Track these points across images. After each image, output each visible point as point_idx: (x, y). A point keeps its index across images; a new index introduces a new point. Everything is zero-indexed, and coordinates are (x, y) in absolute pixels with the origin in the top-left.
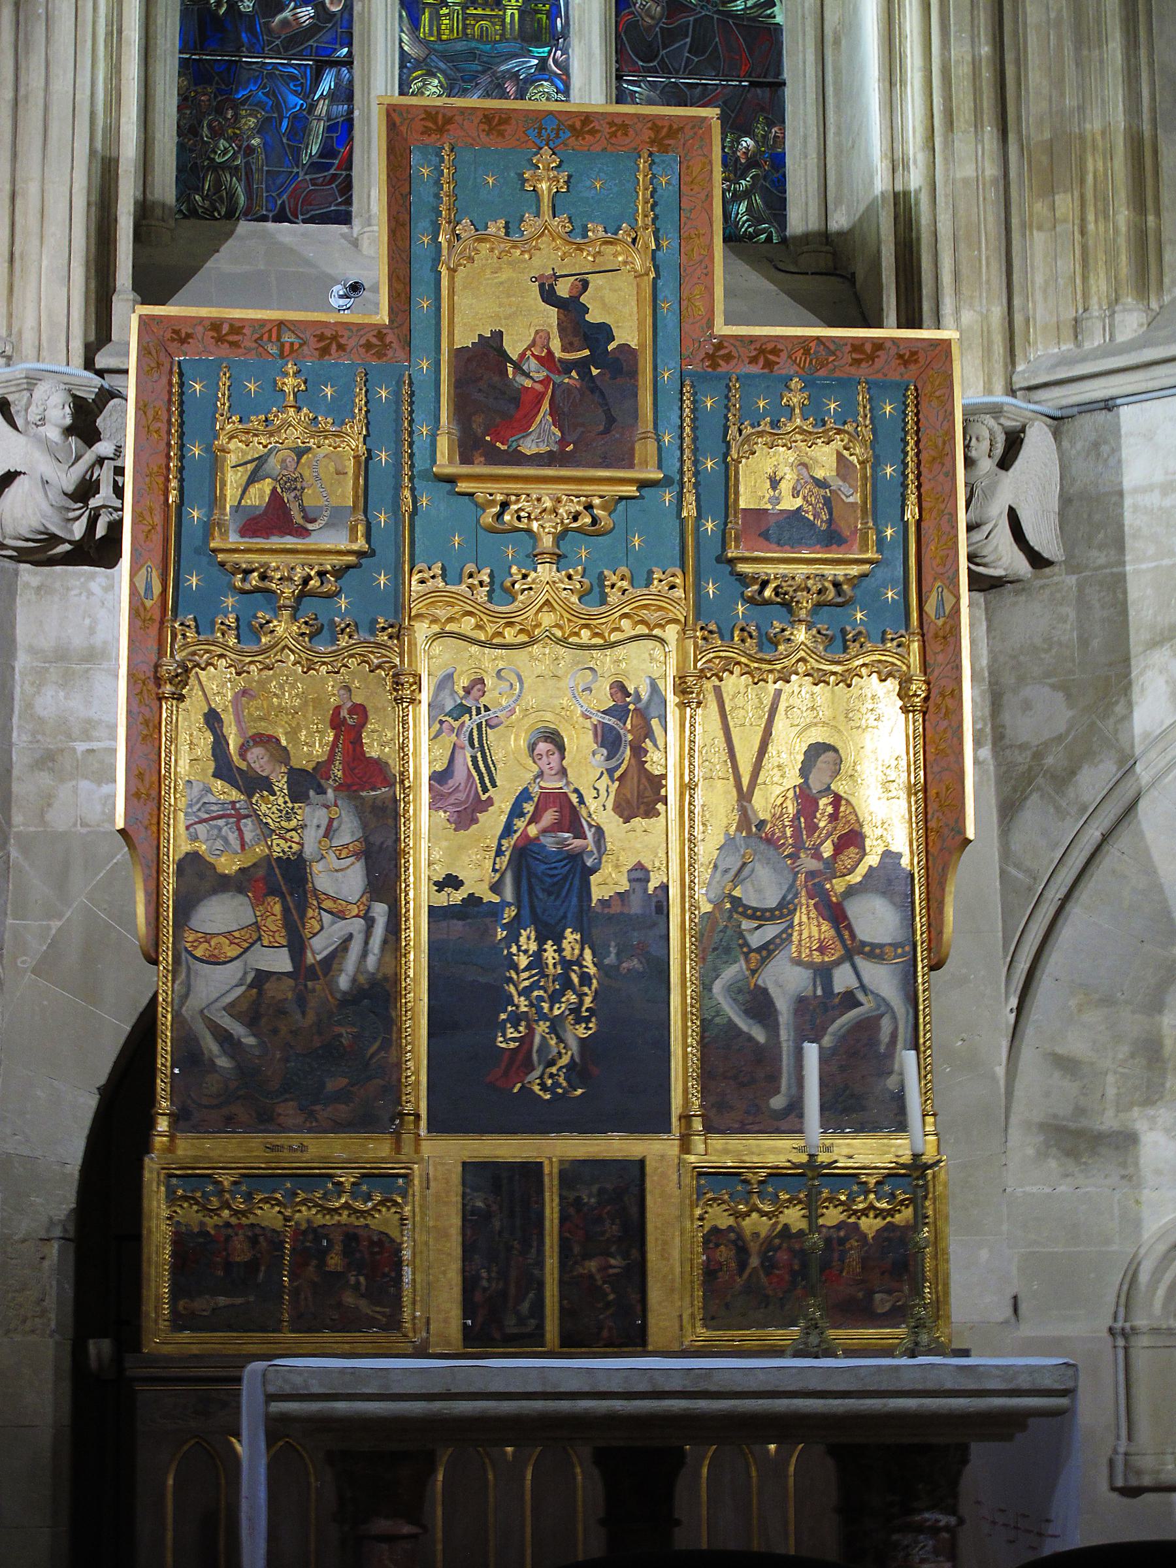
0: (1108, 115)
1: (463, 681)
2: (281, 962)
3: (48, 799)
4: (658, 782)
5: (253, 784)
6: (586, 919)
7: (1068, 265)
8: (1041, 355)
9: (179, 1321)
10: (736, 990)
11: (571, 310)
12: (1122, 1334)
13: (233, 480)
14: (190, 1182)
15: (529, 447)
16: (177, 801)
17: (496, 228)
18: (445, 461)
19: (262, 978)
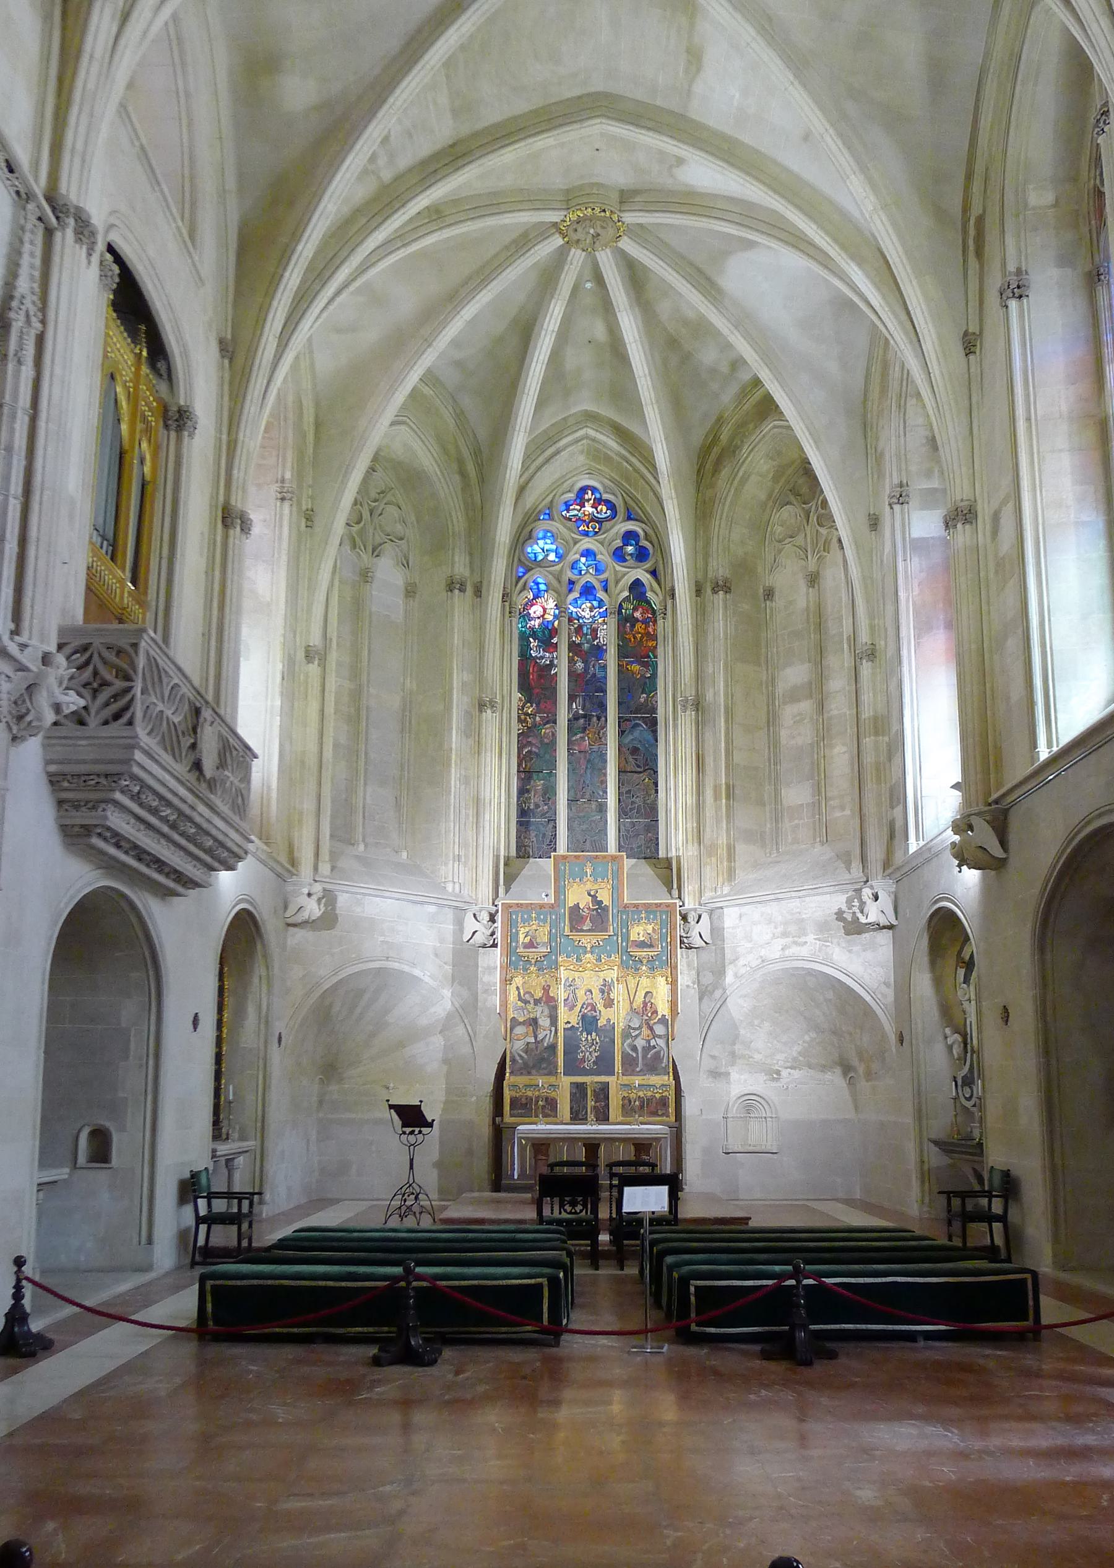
0: (723, 840)
3: (486, 1000)
5: (526, 1002)
8: (708, 895)
9: (512, 1116)
10: (629, 1045)
11: (594, 897)
13: (521, 936)
14: (514, 1086)
15: (585, 928)
17: (578, 880)
18: (567, 931)
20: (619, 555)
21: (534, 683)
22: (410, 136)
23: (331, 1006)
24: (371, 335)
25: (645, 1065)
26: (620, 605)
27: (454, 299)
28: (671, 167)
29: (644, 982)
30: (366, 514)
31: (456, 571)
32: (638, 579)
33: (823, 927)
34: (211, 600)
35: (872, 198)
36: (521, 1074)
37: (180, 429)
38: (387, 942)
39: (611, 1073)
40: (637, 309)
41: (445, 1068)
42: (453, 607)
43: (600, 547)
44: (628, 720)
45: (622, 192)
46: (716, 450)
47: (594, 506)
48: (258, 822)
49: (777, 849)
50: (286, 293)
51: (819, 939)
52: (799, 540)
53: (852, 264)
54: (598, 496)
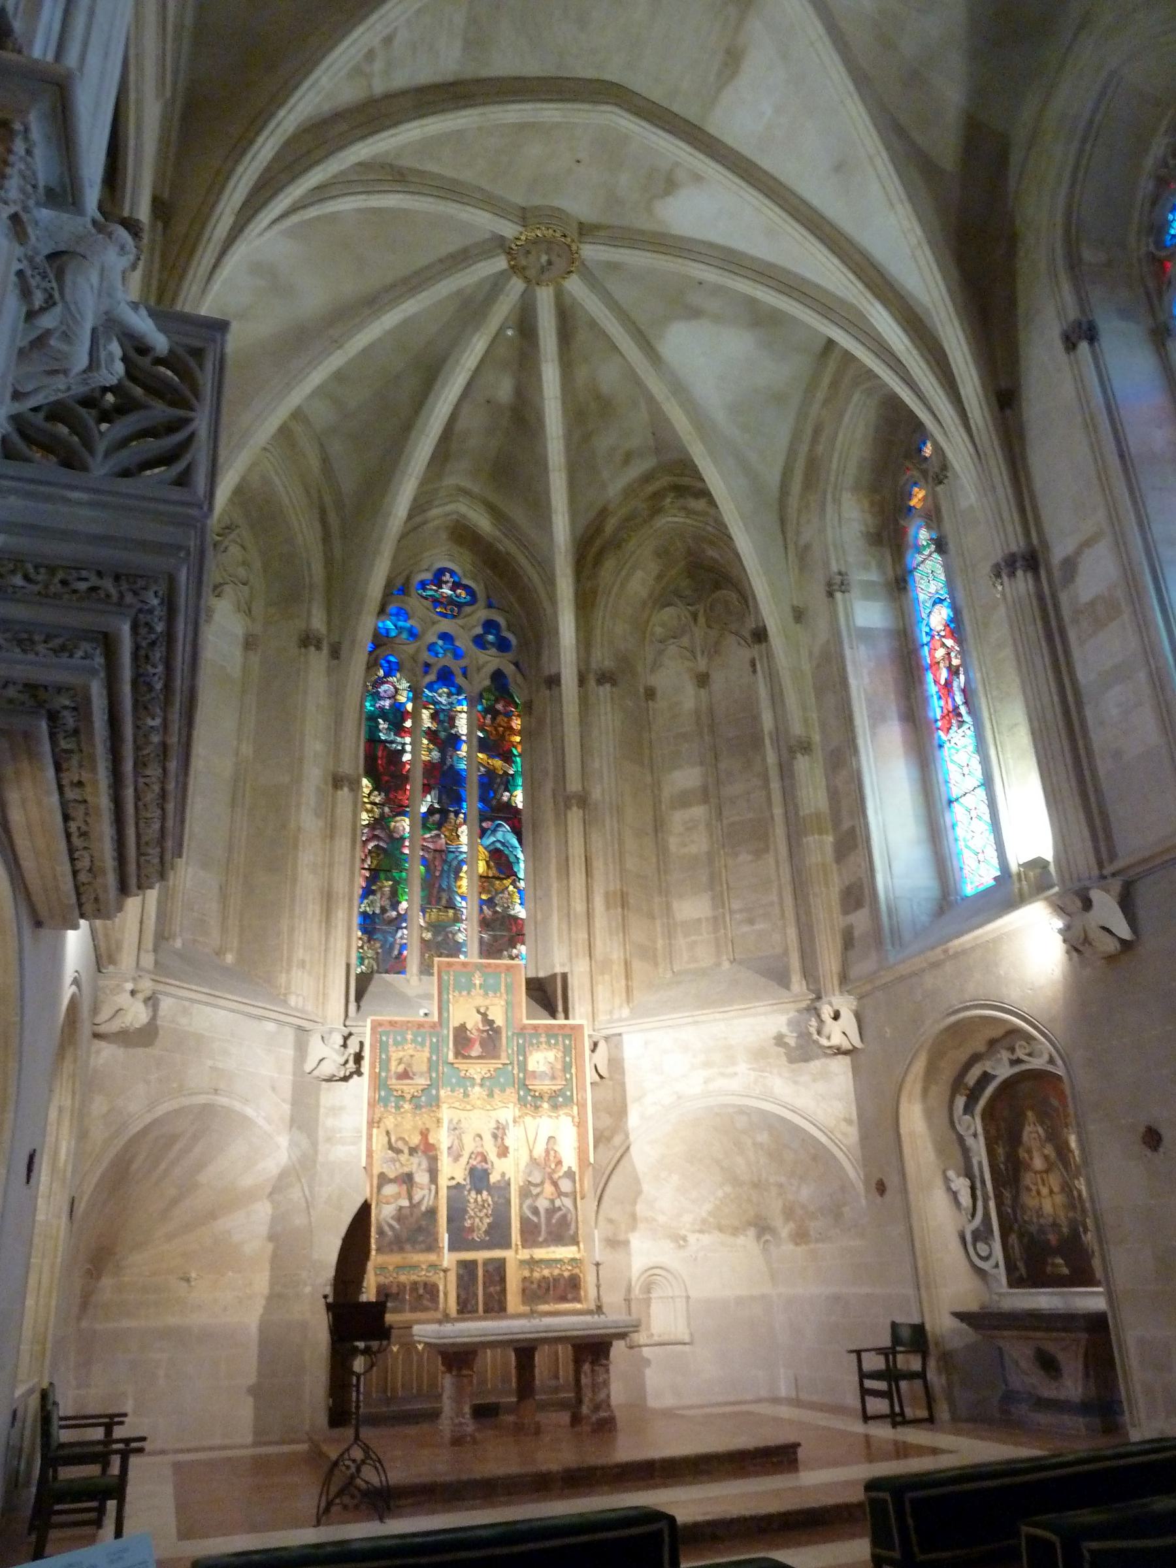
0: (617, 955)
1: (455, 1121)
2: (406, 1203)
4: (507, 1148)
5: (398, 1151)
6: (489, 1188)
11: (484, 1015)
12: (628, 1301)
13: (393, 1064)
15: (473, 1054)
17: (464, 993)
19: (401, 1208)
20: (479, 641)
25: (550, 1233)
27: (373, 303)
33: (758, 1055)
36: (392, 1251)
39: (506, 1244)
41: (270, 1247)
43: (465, 629)
46: (598, 543)
47: (453, 589)
51: (754, 1069)
52: (685, 641)
54: (457, 579)
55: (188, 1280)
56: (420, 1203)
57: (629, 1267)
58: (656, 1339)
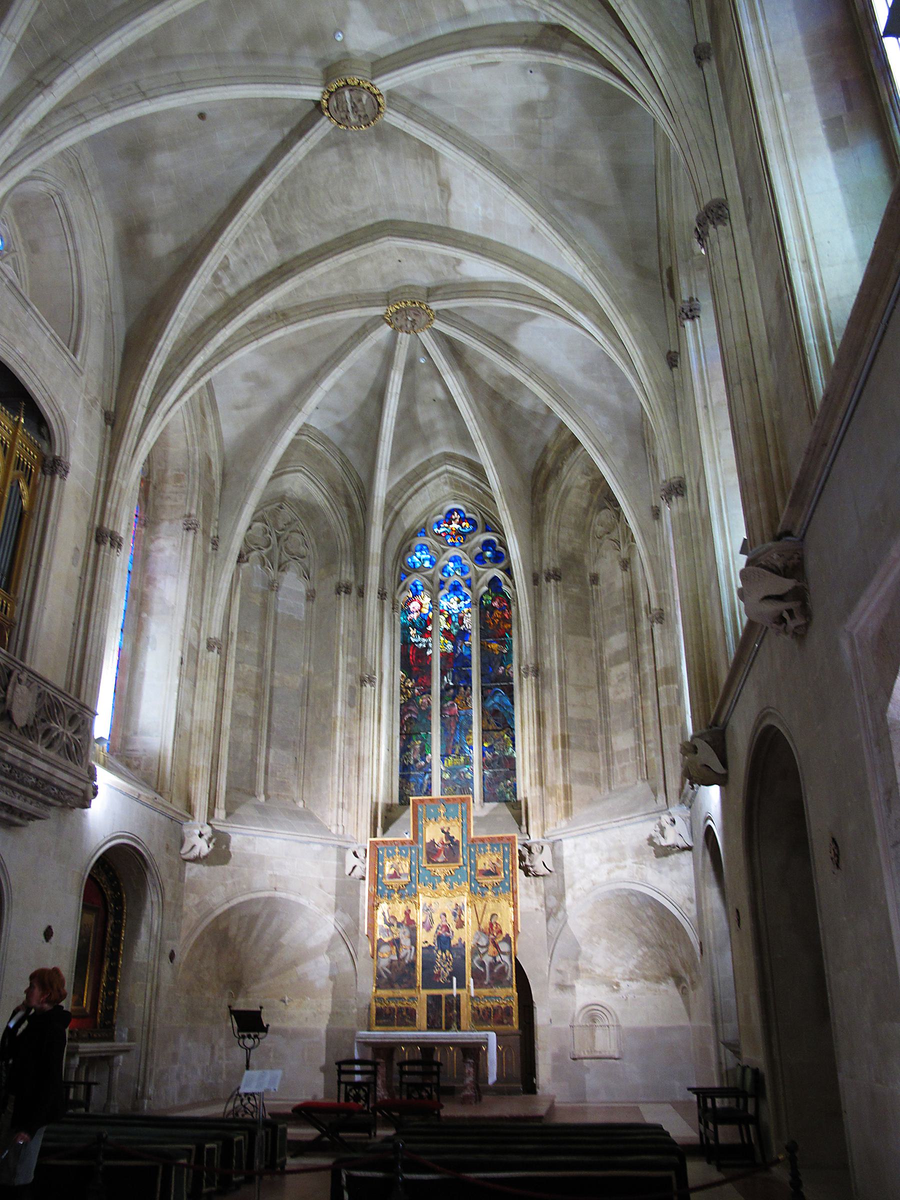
0: (560, 783)
1: (428, 905)
4: (463, 922)
7: (555, 812)
11: (447, 834)
15: (440, 860)
16: (378, 930)
17: (433, 819)
19: (392, 961)
20: (479, 559)
21: (414, 662)
22: (245, 263)
23: (226, 929)
24: (260, 409)
25: (492, 979)
26: (482, 598)
28: (454, 267)
29: (490, 906)
30: (274, 540)
31: (343, 578)
32: (495, 577)
34: (83, 597)
35: (581, 263)
37: (53, 474)
38: (275, 875)
40: (459, 373)
41: (331, 983)
42: (340, 605)
44: (491, 688)
45: (428, 289)
47: (460, 524)
48: (156, 777)
49: (610, 788)
50: (152, 376)
51: (636, 863)
52: (614, 535)
53: (579, 313)
55: (284, 1002)
56: (404, 958)
57: (574, 1004)
58: (598, 1054)
